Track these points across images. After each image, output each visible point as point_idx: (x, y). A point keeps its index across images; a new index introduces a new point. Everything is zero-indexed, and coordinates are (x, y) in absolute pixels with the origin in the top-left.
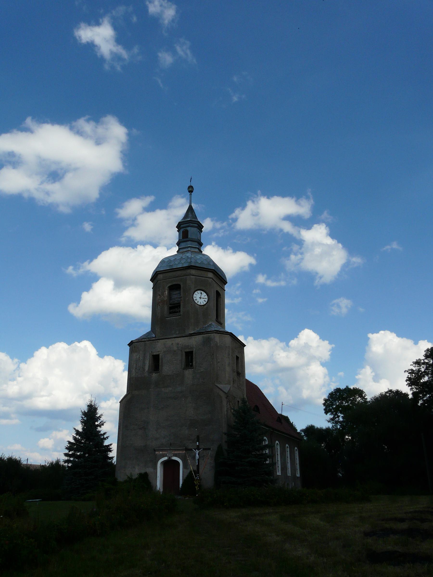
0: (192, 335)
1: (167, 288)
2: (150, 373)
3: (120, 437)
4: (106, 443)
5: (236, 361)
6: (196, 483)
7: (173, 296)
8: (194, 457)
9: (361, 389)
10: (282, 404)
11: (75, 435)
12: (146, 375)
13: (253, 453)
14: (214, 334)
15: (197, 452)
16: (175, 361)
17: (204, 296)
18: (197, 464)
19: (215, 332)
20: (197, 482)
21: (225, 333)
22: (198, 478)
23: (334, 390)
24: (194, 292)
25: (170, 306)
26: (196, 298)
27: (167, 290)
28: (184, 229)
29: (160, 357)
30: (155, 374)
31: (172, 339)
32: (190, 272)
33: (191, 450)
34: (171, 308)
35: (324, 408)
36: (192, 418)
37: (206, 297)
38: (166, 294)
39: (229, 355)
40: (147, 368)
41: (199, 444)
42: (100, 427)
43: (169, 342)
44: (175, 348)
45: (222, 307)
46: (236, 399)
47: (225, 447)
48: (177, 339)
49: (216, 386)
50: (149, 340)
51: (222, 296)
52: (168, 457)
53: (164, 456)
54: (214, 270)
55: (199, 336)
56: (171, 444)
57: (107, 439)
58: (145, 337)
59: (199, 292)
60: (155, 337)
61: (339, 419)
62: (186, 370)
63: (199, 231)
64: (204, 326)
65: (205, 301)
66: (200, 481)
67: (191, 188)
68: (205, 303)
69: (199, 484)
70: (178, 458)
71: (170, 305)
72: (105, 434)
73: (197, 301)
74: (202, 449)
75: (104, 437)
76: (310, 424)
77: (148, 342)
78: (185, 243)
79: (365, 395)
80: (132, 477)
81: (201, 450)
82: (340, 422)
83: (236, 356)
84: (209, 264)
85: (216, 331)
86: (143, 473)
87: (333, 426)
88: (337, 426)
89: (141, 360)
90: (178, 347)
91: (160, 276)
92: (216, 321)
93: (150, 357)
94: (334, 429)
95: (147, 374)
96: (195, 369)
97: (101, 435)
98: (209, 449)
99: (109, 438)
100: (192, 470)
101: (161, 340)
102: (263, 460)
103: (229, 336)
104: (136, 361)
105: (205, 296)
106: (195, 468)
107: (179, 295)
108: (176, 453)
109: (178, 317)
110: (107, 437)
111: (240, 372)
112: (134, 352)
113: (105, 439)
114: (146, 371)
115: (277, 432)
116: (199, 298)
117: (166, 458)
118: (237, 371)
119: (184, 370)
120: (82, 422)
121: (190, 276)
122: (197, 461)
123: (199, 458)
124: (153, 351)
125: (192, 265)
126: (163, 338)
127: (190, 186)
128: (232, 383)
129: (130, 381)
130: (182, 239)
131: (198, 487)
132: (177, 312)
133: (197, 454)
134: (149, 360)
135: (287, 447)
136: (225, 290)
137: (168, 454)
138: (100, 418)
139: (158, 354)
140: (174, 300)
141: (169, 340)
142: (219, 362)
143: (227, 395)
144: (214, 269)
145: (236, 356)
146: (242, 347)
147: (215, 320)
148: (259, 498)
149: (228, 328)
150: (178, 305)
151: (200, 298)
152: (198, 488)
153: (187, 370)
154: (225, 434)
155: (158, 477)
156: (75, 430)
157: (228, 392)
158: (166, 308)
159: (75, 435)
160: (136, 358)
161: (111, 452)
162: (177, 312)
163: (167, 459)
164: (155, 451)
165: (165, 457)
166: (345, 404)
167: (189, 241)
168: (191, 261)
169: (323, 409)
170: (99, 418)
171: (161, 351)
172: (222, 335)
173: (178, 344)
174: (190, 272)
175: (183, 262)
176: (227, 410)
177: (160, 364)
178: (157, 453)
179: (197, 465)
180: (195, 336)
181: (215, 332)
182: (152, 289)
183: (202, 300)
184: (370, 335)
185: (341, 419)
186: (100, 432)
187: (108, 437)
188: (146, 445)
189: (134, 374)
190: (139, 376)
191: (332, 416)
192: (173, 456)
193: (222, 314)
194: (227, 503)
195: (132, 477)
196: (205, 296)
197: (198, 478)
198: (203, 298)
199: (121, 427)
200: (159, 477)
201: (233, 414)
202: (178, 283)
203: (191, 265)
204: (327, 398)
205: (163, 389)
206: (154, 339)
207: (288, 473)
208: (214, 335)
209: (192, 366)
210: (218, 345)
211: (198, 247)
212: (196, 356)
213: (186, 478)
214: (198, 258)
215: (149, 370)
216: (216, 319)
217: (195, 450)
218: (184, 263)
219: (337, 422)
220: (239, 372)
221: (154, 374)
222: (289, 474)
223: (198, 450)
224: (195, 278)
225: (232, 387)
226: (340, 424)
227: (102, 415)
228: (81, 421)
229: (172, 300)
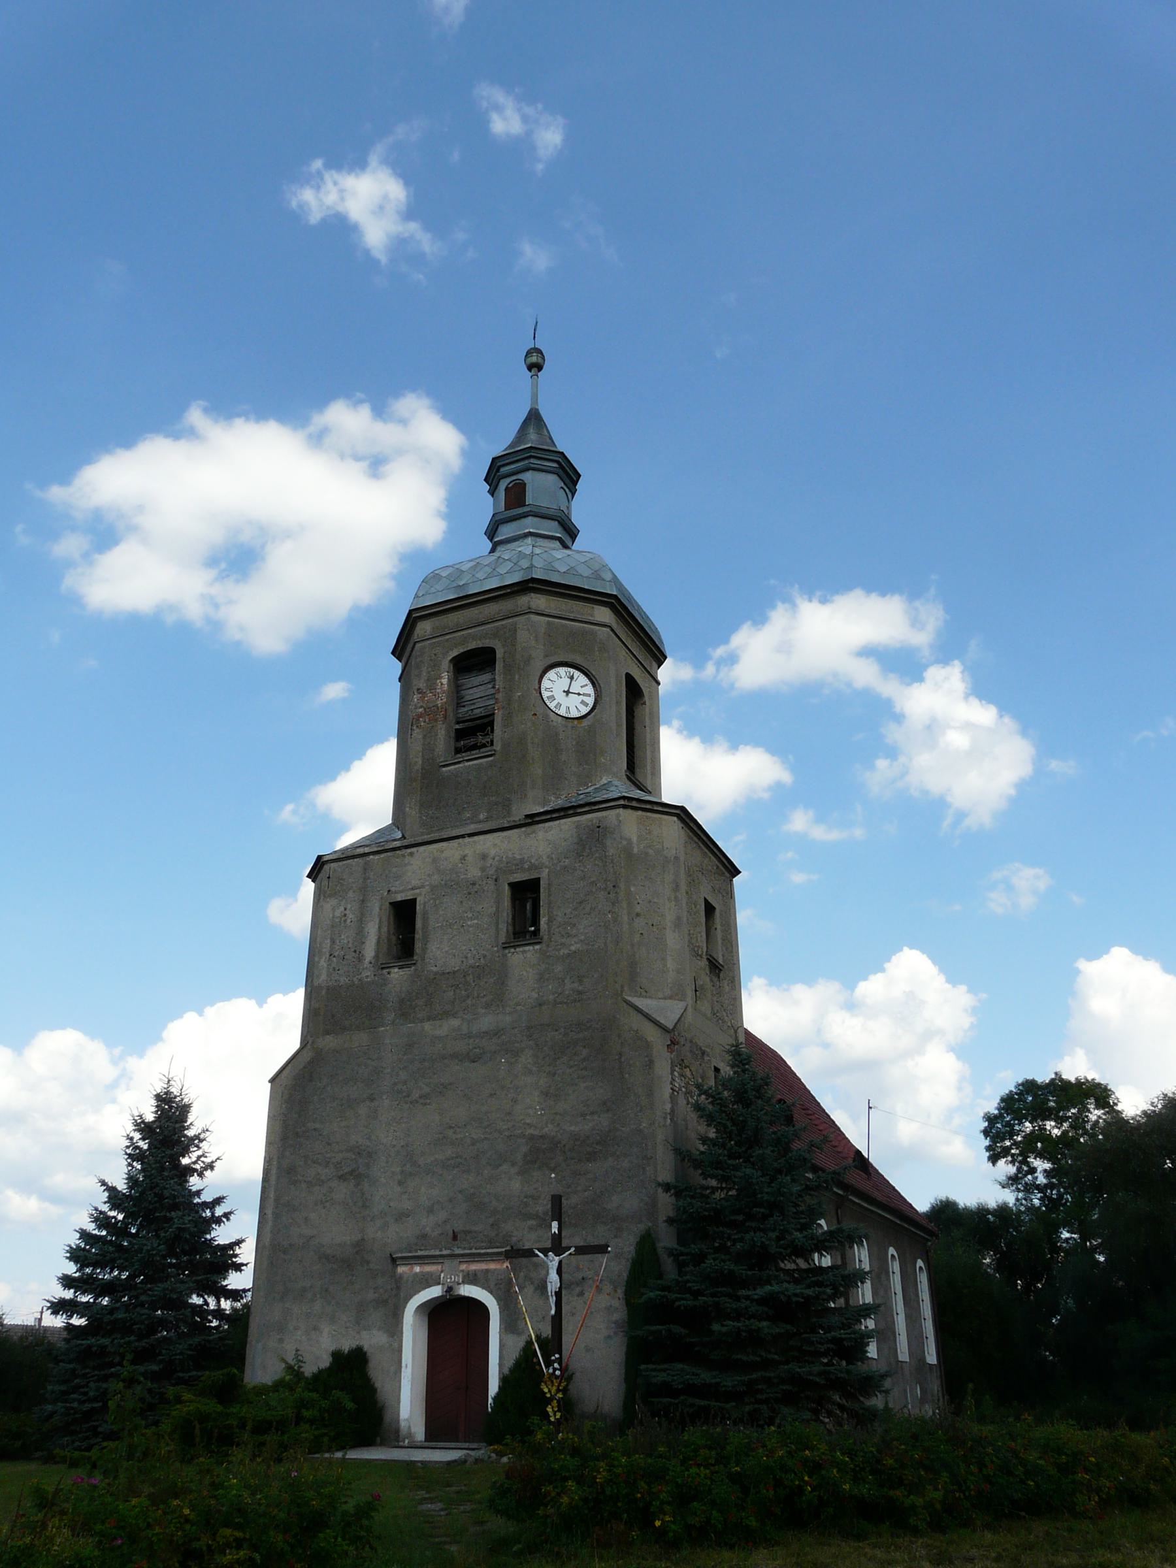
0: (537, 819)
1: (446, 664)
2: (383, 968)
3: (269, 1212)
4: (221, 1235)
5: (703, 919)
6: (550, 1391)
7: (471, 691)
8: (542, 1287)
9: (1102, 1083)
10: (870, 1108)
11: (105, 1208)
12: (367, 977)
13: (782, 1265)
14: (617, 811)
15: (553, 1261)
16: (471, 919)
17: (582, 687)
18: (553, 1312)
19: (622, 802)
20: (553, 1391)
21: (660, 809)
22: (558, 1373)
23: (1016, 1087)
24: (541, 677)
25: (457, 727)
26: (551, 694)
27: (448, 672)
28: (511, 482)
29: (418, 908)
30: (401, 972)
31: (461, 840)
32: (529, 602)
33: (530, 1253)
34: (460, 735)
35: (987, 1142)
36: (536, 1132)
37: (590, 689)
38: (442, 684)
39: (677, 888)
40: (369, 952)
41: (560, 1229)
42: (201, 1175)
43: (450, 852)
44: (474, 873)
45: (648, 736)
46: (706, 1058)
47: (666, 1239)
48: (481, 837)
49: (626, 1002)
50: (380, 849)
51: (646, 698)
52: (443, 1284)
53: (427, 1281)
54: (615, 597)
55: (562, 821)
56: (455, 1237)
57: (224, 1220)
58: (368, 842)
59: (562, 671)
60: (404, 837)
61: (1037, 1178)
62: (512, 950)
63: (562, 488)
64: (580, 792)
65: (586, 705)
66: (563, 1384)
67: (535, 354)
68: (584, 710)
69: (560, 1395)
70: (483, 1288)
71: (458, 723)
72: (218, 1201)
73: (555, 703)
74: (573, 1250)
75: (213, 1214)
76: (942, 1196)
77: (377, 857)
78: (514, 525)
79: (1116, 1101)
80: (300, 1367)
81: (570, 1254)
82: (1040, 1188)
83: (706, 901)
84: (597, 576)
85: (624, 798)
86: (346, 1352)
87: (1017, 1200)
88: (1031, 1200)
89: (349, 921)
90: (483, 869)
91: (424, 628)
92: (629, 778)
93: (381, 909)
94: (1022, 1209)
95: (369, 974)
96: (548, 946)
97: (205, 1205)
98: (602, 1249)
99: (232, 1217)
100: (533, 1337)
101: (422, 848)
102: (829, 1291)
103: (675, 818)
104: (333, 926)
105: (587, 685)
106: (547, 1331)
107: (490, 686)
108: (475, 1271)
109: (487, 762)
110: (227, 1215)
111: (721, 962)
112: (325, 896)
113: (218, 1221)
114: (367, 960)
115: (857, 1201)
116: (564, 691)
117: (435, 1292)
118: (710, 956)
119: (507, 951)
120: (130, 1156)
121: (527, 616)
122: (554, 1298)
123: (560, 1288)
124: (393, 889)
125: (534, 576)
126: (426, 838)
127: (531, 349)
128: (690, 993)
129: (310, 1002)
130: (506, 510)
131: (558, 1411)
132: (484, 746)
133: (550, 1271)
134: (377, 921)
135: (893, 1256)
136: (658, 683)
137: (442, 1275)
138: (201, 1141)
139: (411, 897)
140: (474, 704)
141: (454, 843)
142: (638, 915)
143: (673, 1036)
144: (615, 593)
145: (706, 901)
146: (727, 875)
147: (624, 774)
148: (847, 1487)
149: (669, 794)
150: (486, 720)
151: (567, 692)
152: (558, 1415)
153: (518, 949)
154: (667, 1187)
155: (406, 1365)
156: (104, 1188)
157: (675, 1027)
158: (442, 735)
159: (105, 1208)
160: (333, 917)
161: (241, 1271)
162: (484, 744)
163: (440, 1294)
164: (394, 1260)
165: (431, 1286)
166: (1053, 1129)
167: (528, 516)
168: (532, 566)
169: (983, 1147)
170: (196, 1142)
171: (423, 886)
172: (649, 814)
173: (484, 857)
174: (529, 602)
175: (502, 570)
176: (672, 1097)
177: (419, 935)
178: (401, 1270)
179: (553, 1317)
180: (547, 824)
181: (622, 802)
182: (400, 681)
183: (573, 701)
184: (1082, 965)
185: (1041, 1180)
186: (198, 1193)
187: (230, 1213)
188: (363, 1239)
189: (324, 977)
190: (342, 979)
191: (1012, 1170)
192: (464, 1282)
193: (649, 761)
194: (667, 1518)
195: (301, 1367)
196: (587, 685)
197: (555, 1369)
198: (579, 694)
199: (274, 1171)
200: (410, 1366)
201: (698, 1108)
202: (487, 643)
203: (532, 578)
204: (996, 1112)
205: (427, 1026)
206: (398, 845)
207: (899, 1350)
208: (618, 815)
209: (535, 935)
210: (635, 850)
211: (559, 535)
212: (550, 895)
213: (512, 1371)
214: (560, 557)
215: (377, 957)
216: (626, 771)
217: (545, 1252)
218: (507, 573)
219: (1029, 1188)
220: (719, 963)
221: (396, 970)
222: (904, 1355)
223: (556, 1256)
224: (548, 621)
225: (690, 1010)
226: (1039, 1195)
227: (207, 1130)
228: (126, 1154)
229: (464, 706)
